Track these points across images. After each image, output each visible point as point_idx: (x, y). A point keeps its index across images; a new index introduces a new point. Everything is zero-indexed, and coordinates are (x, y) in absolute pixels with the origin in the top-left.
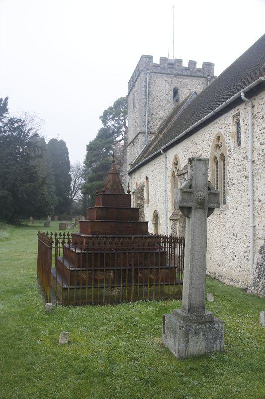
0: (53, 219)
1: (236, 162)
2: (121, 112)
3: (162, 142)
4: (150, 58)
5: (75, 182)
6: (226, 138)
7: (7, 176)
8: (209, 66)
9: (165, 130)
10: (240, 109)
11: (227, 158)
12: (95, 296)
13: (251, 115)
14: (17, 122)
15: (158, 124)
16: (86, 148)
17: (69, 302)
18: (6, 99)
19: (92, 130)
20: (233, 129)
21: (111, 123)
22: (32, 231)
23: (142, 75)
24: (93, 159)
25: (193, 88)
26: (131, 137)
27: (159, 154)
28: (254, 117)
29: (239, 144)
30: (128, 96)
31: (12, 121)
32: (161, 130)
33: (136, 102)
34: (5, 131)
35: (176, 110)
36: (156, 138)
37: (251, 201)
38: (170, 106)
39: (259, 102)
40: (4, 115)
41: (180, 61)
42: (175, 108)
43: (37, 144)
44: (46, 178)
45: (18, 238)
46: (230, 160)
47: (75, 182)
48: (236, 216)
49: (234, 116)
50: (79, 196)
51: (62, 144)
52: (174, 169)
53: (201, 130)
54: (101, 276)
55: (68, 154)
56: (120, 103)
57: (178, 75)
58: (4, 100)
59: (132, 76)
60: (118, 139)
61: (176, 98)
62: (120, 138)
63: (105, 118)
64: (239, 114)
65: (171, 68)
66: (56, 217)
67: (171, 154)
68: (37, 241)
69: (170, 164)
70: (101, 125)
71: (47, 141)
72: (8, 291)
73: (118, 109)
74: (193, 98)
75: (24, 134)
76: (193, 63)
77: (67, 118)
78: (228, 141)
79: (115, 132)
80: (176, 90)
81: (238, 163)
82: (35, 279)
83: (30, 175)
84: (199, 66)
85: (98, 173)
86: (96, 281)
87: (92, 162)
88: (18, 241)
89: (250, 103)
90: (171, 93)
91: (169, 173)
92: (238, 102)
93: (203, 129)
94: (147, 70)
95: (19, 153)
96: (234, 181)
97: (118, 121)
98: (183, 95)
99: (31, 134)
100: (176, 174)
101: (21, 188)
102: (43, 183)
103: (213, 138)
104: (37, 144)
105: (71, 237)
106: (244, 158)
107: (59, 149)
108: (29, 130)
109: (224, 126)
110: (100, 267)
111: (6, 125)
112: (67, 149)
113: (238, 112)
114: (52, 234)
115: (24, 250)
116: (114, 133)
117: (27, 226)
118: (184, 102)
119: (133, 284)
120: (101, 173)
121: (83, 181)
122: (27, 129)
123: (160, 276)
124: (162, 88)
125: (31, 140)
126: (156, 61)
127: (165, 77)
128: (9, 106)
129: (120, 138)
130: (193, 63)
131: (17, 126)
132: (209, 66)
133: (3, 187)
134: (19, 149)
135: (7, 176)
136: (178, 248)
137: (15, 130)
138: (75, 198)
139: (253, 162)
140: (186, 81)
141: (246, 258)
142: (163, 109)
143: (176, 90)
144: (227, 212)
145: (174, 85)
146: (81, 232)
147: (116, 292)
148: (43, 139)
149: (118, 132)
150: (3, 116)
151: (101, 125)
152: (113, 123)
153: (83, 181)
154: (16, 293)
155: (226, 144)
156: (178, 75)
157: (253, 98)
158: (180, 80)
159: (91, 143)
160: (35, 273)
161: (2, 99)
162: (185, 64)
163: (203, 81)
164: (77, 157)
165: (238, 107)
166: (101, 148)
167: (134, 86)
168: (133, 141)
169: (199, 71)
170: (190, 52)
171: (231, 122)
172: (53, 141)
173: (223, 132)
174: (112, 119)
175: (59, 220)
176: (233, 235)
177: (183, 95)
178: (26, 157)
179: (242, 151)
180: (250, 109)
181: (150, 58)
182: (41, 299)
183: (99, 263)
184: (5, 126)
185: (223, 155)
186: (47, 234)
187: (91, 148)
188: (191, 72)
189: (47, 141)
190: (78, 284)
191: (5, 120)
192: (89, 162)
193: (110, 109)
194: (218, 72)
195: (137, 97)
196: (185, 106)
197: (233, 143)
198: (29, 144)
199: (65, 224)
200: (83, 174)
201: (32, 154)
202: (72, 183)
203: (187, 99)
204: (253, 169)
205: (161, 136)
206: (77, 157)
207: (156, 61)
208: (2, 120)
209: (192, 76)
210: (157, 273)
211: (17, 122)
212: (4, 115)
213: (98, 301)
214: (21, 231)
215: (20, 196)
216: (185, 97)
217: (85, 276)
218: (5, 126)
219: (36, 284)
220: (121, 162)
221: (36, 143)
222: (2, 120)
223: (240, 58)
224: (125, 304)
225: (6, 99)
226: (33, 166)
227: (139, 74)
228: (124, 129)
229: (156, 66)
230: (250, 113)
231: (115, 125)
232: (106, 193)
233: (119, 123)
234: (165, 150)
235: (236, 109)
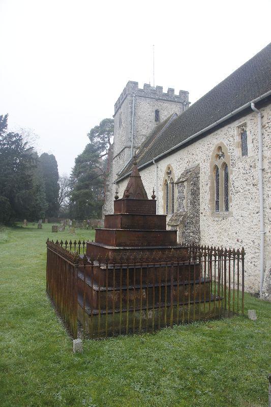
0: (44, 222)
1: (242, 171)
2: (106, 131)
3: (150, 154)
4: (136, 84)
5: (62, 190)
6: (228, 147)
7: (6, 183)
8: (184, 94)
9: (151, 145)
10: (247, 119)
11: (230, 168)
12: (131, 322)
13: (257, 127)
14: (15, 136)
15: (141, 141)
16: (74, 160)
17: (101, 332)
18: (6, 116)
19: (80, 145)
20: (238, 139)
21: (97, 140)
22: (28, 232)
23: (129, 97)
24: (81, 170)
25: (170, 111)
26: (116, 151)
27: (152, 164)
28: (263, 127)
29: (245, 151)
30: (114, 116)
31: (10, 136)
32: (145, 145)
33: (123, 121)
34: (4, 144)
35: (158, 128)
36: (140, 153)
37: (261, 208)
38: (153, 126)
39: (267, 112)
40: (4, 130)
41: (160, 88)
42: (156, 127)
43: (32, 156)
44: (40, 185)
45: (16, 241)
46: (234, 169)
47: (62, 190)
48: (241, 222)
49: (239, 127)
50: (67, 200)
51: (53, 157)
52: (167, 178)
53: (199, 141)
54: (132, 296)
55: (57, 166)
56: (105, 123)
57: (159, 99)
58: (4, 117)
59: (119, 99)
60: (103, 153)
61: (157, 118)
62: (104, 153)
63: (92, 135)
64: (245, 125)
65: (154, 94)
66: (46, 220)
67: (163, 165)
68: (46, 249)
69: (162, 175)
70: (89, 142)
71: (39, 155)
72: (17, 313)
73: (105, 128)
74: (174, 118)
75: (21, 147)
76: (171, 91)
77: (59, 137)
78: (231, 151)
79: (101, 148)
80: (157, 112)
81: (245, 172)
82: (44, 292)
83: (26, 183)
84: (177, 93)
85: (85, 182)
86: (125, 301)
87: (80, 173)
88: (17, 243)
89: (259, 113)
90: (154, 114)
91: (161, 182)
92: (248, 111)
93: (201, 140)
94: (132, 94)
95: (16, 163)
96: (239, 189)
97: (103, 139)
98: (163, 117)
99: (27, 147)
100: (169, 182)
101: (18, 194)
102: (38, 190)
103: (213, 148)
104: (32, 156)
105: (85, 245)
106: (251, 166)
107: (50, 162)
108: (26, 143)
109: (228, 137)
110: (130, 285)
111: (5, 138)
112: (56, 162)
113: (245, 122)
114: (66, 243)
115: (25, 254)
116: (99, 148)
117: (22, 228)
118: (166, 122)
119: (172, 303)
120: (87, 182)
121: (69, 190)
122: (24, 143)
123: (195, 292)
124: (146, 110)
125: (27, 152)
126: (141, 86)
127: (148, 100)
128: (8, 122)
129: (104, 153)
130: (171, 91)
131: (15, 141)
132: (184, 94)
133: (2, 192)
134: (16, 160)
135: (6, 183)
136: (224, 261)
137: (13, 143)
138: (62, 203)
139: (263, 170)
140: (166, 104)
141: (253, 263)
142: (146, 127)
143: (157, 112)
144: (230, 218)
145: (156, 108)
146: (97, 241)
147: (151, 314)
148: (36, 153)
149: (103, 147)
150: (2, 131)
151: (89, 142)
152: (99, 140)
153: (69, 190)
154: (27, 315)
155: (229, 154)
156: (159, 99)
157: (262, 109)
158: (162, 104)
159: (79, 156)
160: (43, 284)
161: (2, 116)
162: (165, 91)
163: (179, 105)
164: (66, 169)
165: (244, 118)
166: (87, 162)
167: (120, 107)
168: (119, 154)
169: (177, 97)
170: (166, 81)
171: (236, 132)
172: (45, 155)
173: (225, 142)
174: (98, 136)
175: (49, 222)
176: (238, 241)
177: (163, 117)
178: (22, 167)
179: (248, 160)
180: (259, 119)
181: (136, 84)
182: (58, 326)
183: (128, 281)
184: (4, 139)
185: (225, 166)
186: (62, 243)
187: (79, 161)
188: (169, 98)
189: (39, 155)
190: (111, 308)
191: (4, 135)
192: (77, 172)
193: (97, 128)
194: (193, 99)
195: (123, 117)
196: (167, 125)
197: (238, 152)
198: (24, 156)
199: (57, 227)
200: (70, 184)
201: (28, 165)
202: (60, 191)
203: (169, 119)
204: (263, 177)
205: (146, 150)
206: (66, 169)
207: (141, 86)
208: (2, 134)
209: (170, 101)
210: (192, 289)
211: (15, 136)
212: (4, 130)
213: (131, 330)
214: (17, 233)
215: (16, 201)
216: (165, 119)
217: (114, 297)
218: (4, 139)
219: (47, 298)
220: (107, 174)
221: (29, 157)
222: (2, 134)
223: (215, 88)
224: (166, 330)
225: (6, 116)
226: (28, 175)
227: (126, 97)
228: (108, 145)
229: (141, 90)
230: (259, 123)
231: (101, 141)
232: (130, 198)
233: (103, 140)
234: (157, 161)
235: (241, 120)
